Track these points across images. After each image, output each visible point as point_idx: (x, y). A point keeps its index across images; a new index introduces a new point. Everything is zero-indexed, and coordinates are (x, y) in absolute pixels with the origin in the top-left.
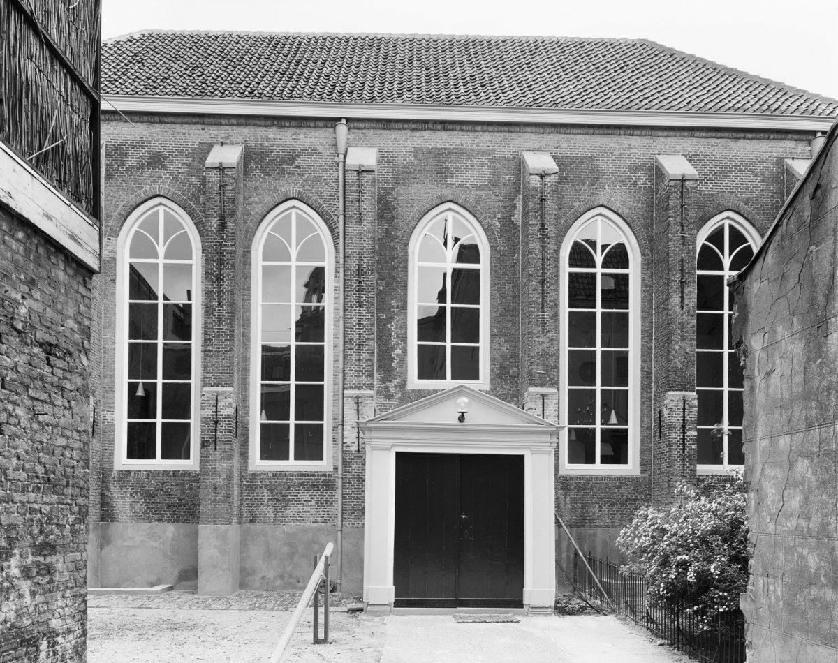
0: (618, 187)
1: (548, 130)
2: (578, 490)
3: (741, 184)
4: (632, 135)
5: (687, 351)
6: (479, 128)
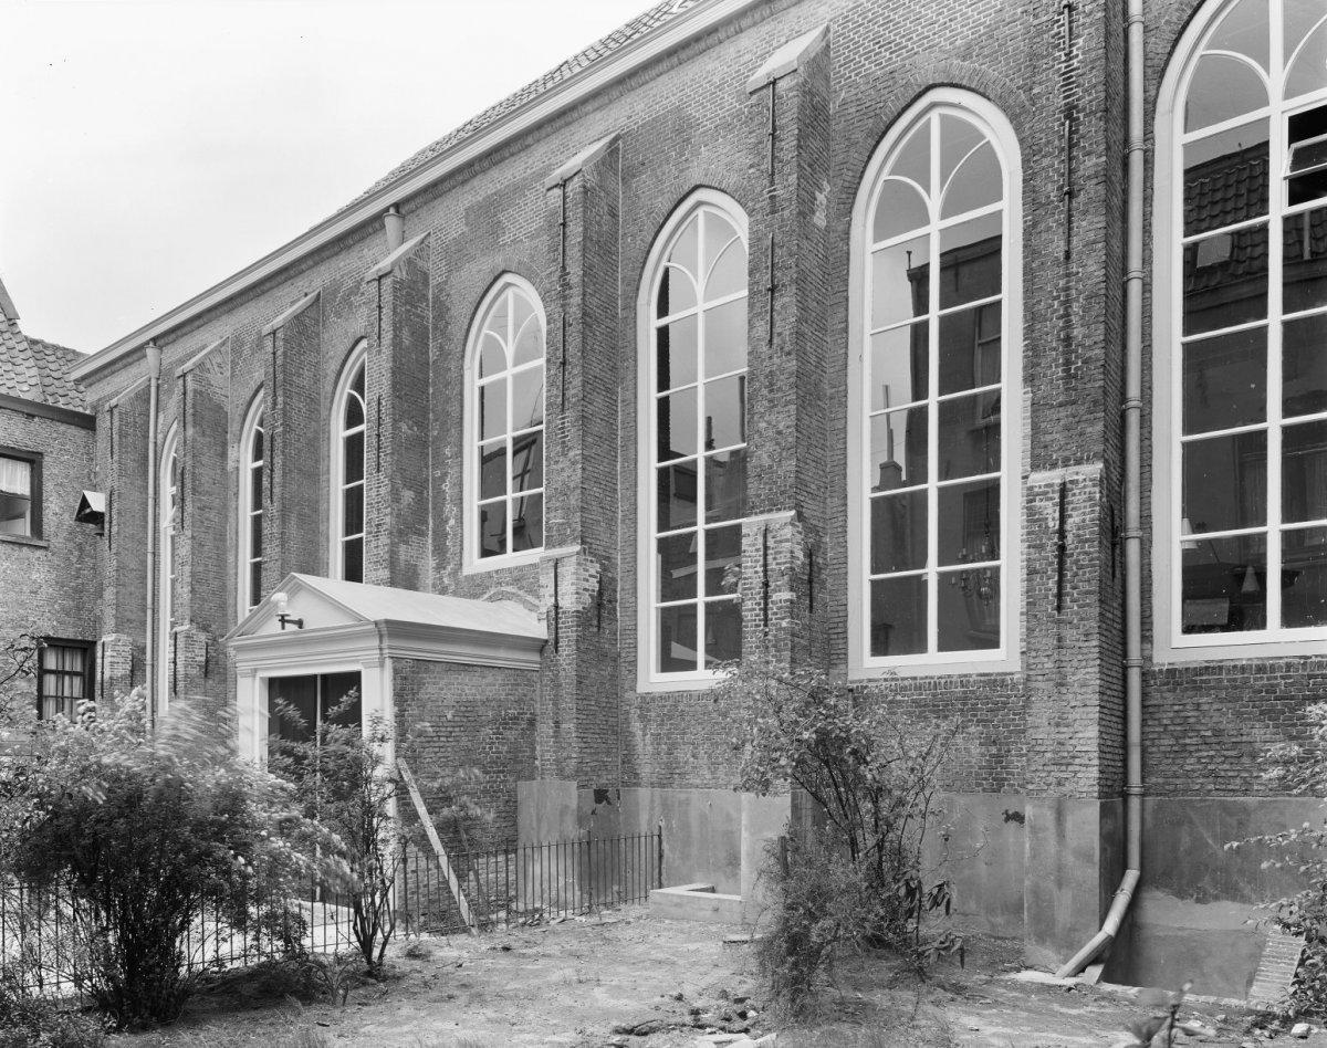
0: (721, 140)
1: (615, 93)
2: (663, 721)
3: (951, 20)
4: (741, 31)
5: (781, 428)
6: (530, 140)
